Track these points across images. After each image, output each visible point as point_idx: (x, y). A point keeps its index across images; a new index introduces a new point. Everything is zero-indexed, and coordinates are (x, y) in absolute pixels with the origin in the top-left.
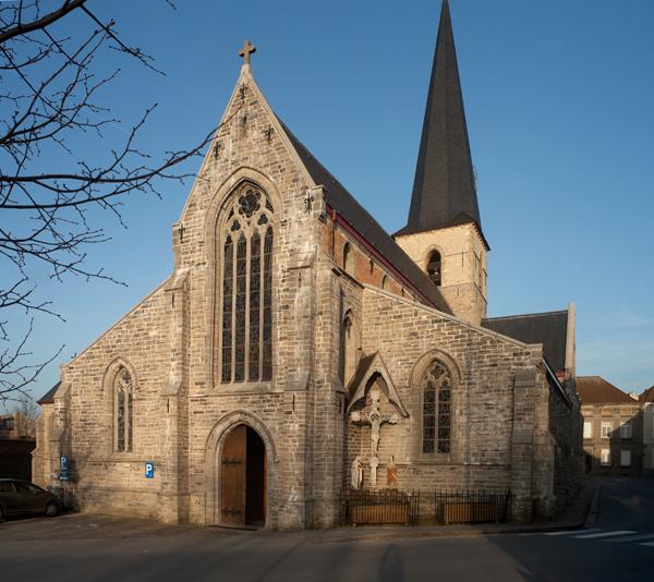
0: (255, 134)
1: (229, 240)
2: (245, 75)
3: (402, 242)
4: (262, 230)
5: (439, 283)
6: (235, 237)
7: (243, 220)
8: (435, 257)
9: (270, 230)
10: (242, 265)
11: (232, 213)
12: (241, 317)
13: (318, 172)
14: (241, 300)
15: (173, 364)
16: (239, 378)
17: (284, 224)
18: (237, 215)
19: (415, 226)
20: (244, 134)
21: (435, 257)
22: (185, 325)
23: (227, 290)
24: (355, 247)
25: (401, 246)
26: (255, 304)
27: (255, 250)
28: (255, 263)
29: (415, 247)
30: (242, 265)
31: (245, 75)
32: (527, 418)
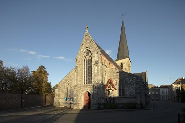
0: (88, 41)
1: (85, 60)
2: (87, 31)
3: (116, 62)
4: (90, 58)
5: (122, 68)
6: (86, 60)
7: (87, 57)
8: (122, 64)
9: (91, 58)
10: (87, 64)
11: (85, 56)
12: (87, 73)
13: (99, 47)
14: (87, 70)
15: (76, 82)
16: (87, 83)
17: (93, 56)
18: (86, 56)
19: (119, 58)
20: (87, 42)
21: (122, 64)
22: (77, 75)
23: (84, 69)
24: (106, 60)
25: (117, 63)
26: (89, 71)
27: (89, 62)
28: (89, 64)
29: (118, 63)
30: (87, 64)
31: (87, 31)
32: (139, 89)
